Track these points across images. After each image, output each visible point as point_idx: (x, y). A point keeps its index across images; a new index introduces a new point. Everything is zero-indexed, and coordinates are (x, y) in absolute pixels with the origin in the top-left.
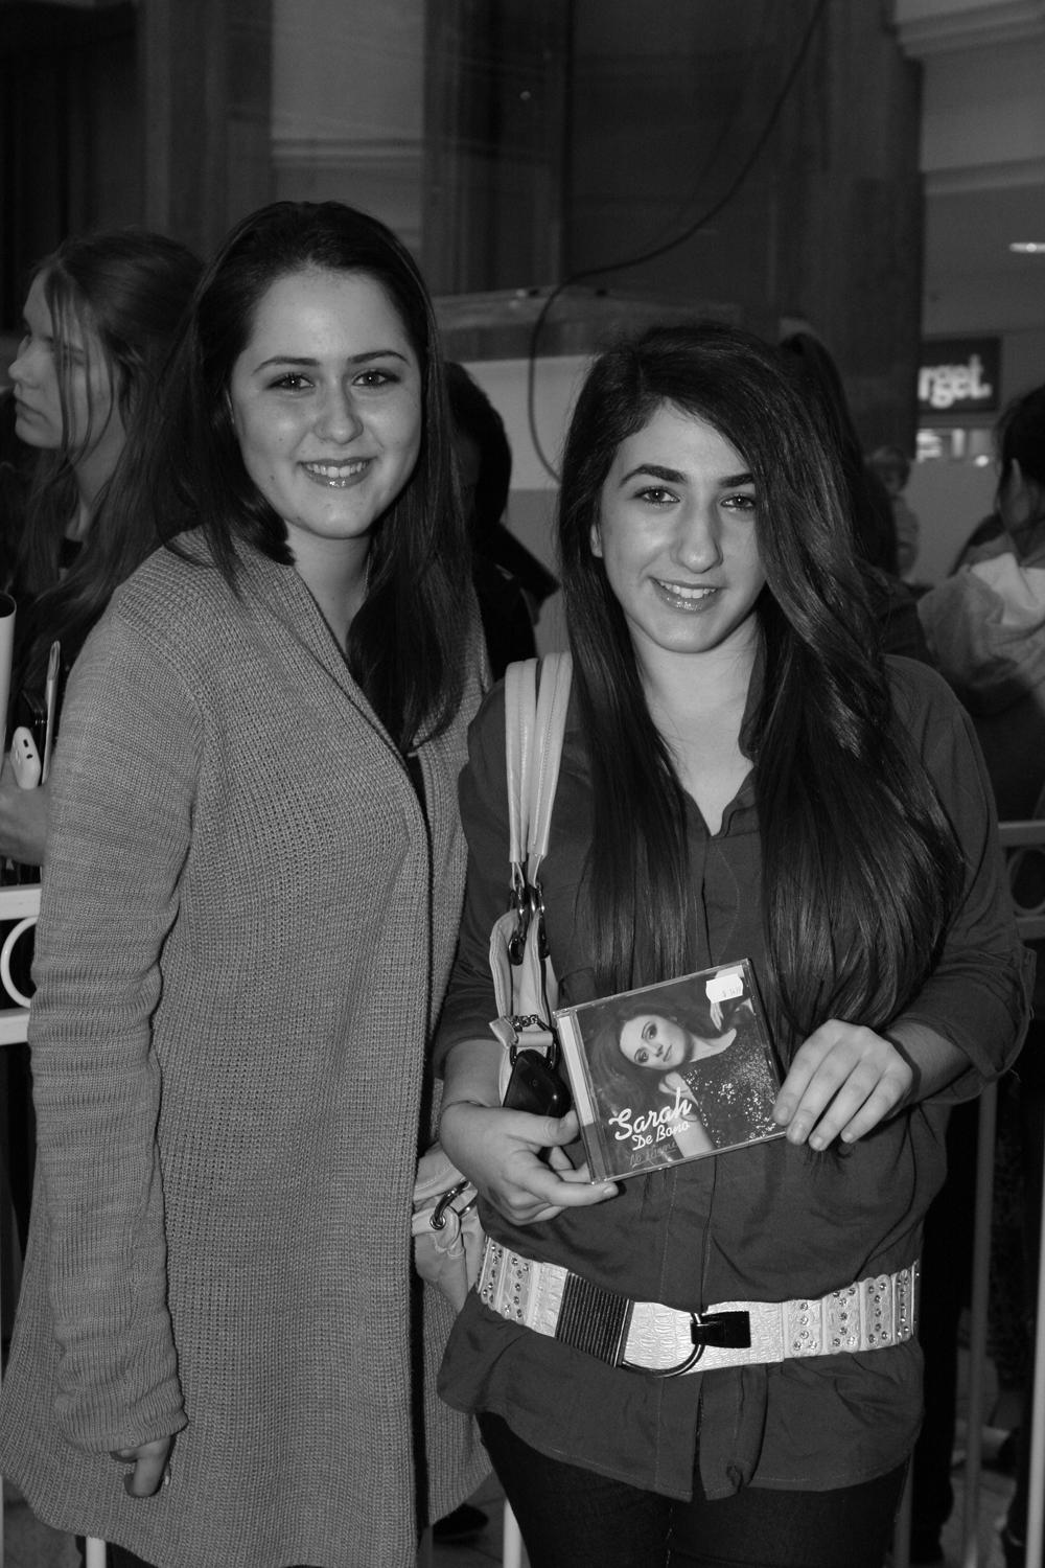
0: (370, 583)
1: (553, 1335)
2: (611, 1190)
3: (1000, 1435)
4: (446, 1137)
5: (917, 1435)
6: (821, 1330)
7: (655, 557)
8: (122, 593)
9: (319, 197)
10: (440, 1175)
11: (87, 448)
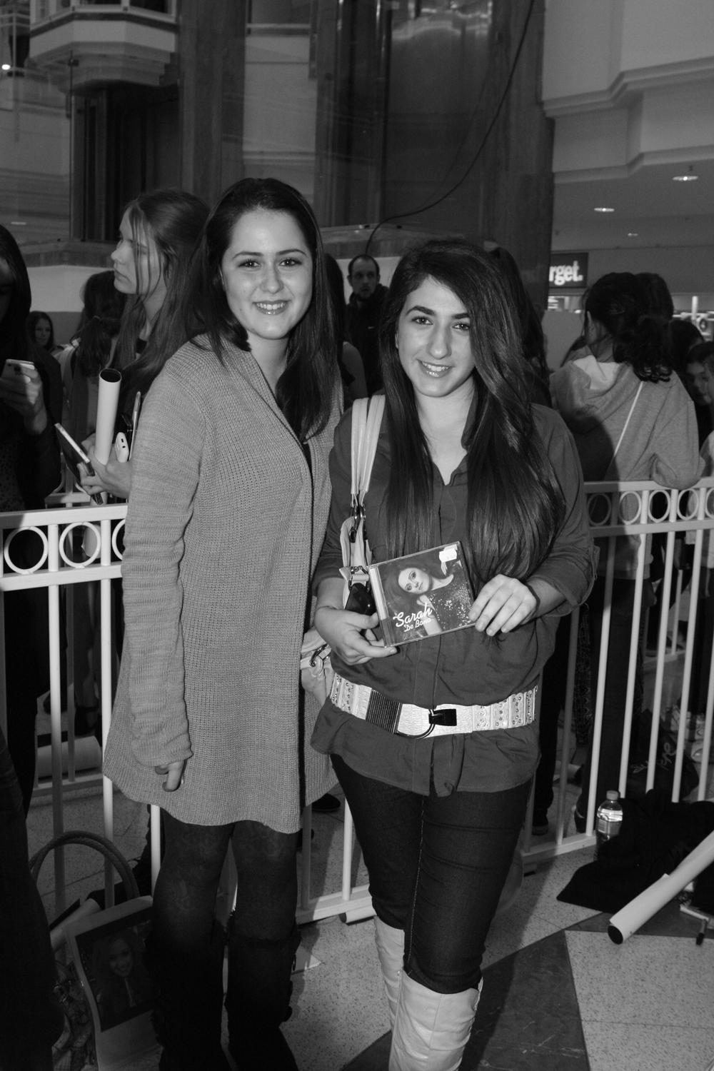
0: (288, 361)
1: (364, 719)
2: (394, 651)
3: (576, 768)
4: (317, 623)
5: (538, 763)
6: (490, 718)
7: (419, 350)
8: (169, 364)
9: (265, 177)
10: (314, 641)
11: (148, 294)
